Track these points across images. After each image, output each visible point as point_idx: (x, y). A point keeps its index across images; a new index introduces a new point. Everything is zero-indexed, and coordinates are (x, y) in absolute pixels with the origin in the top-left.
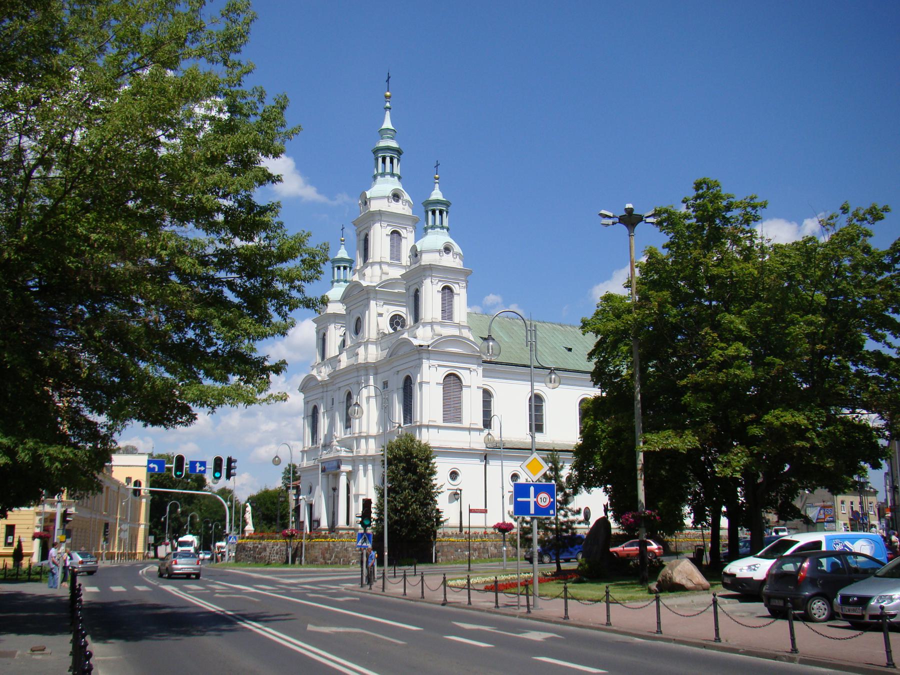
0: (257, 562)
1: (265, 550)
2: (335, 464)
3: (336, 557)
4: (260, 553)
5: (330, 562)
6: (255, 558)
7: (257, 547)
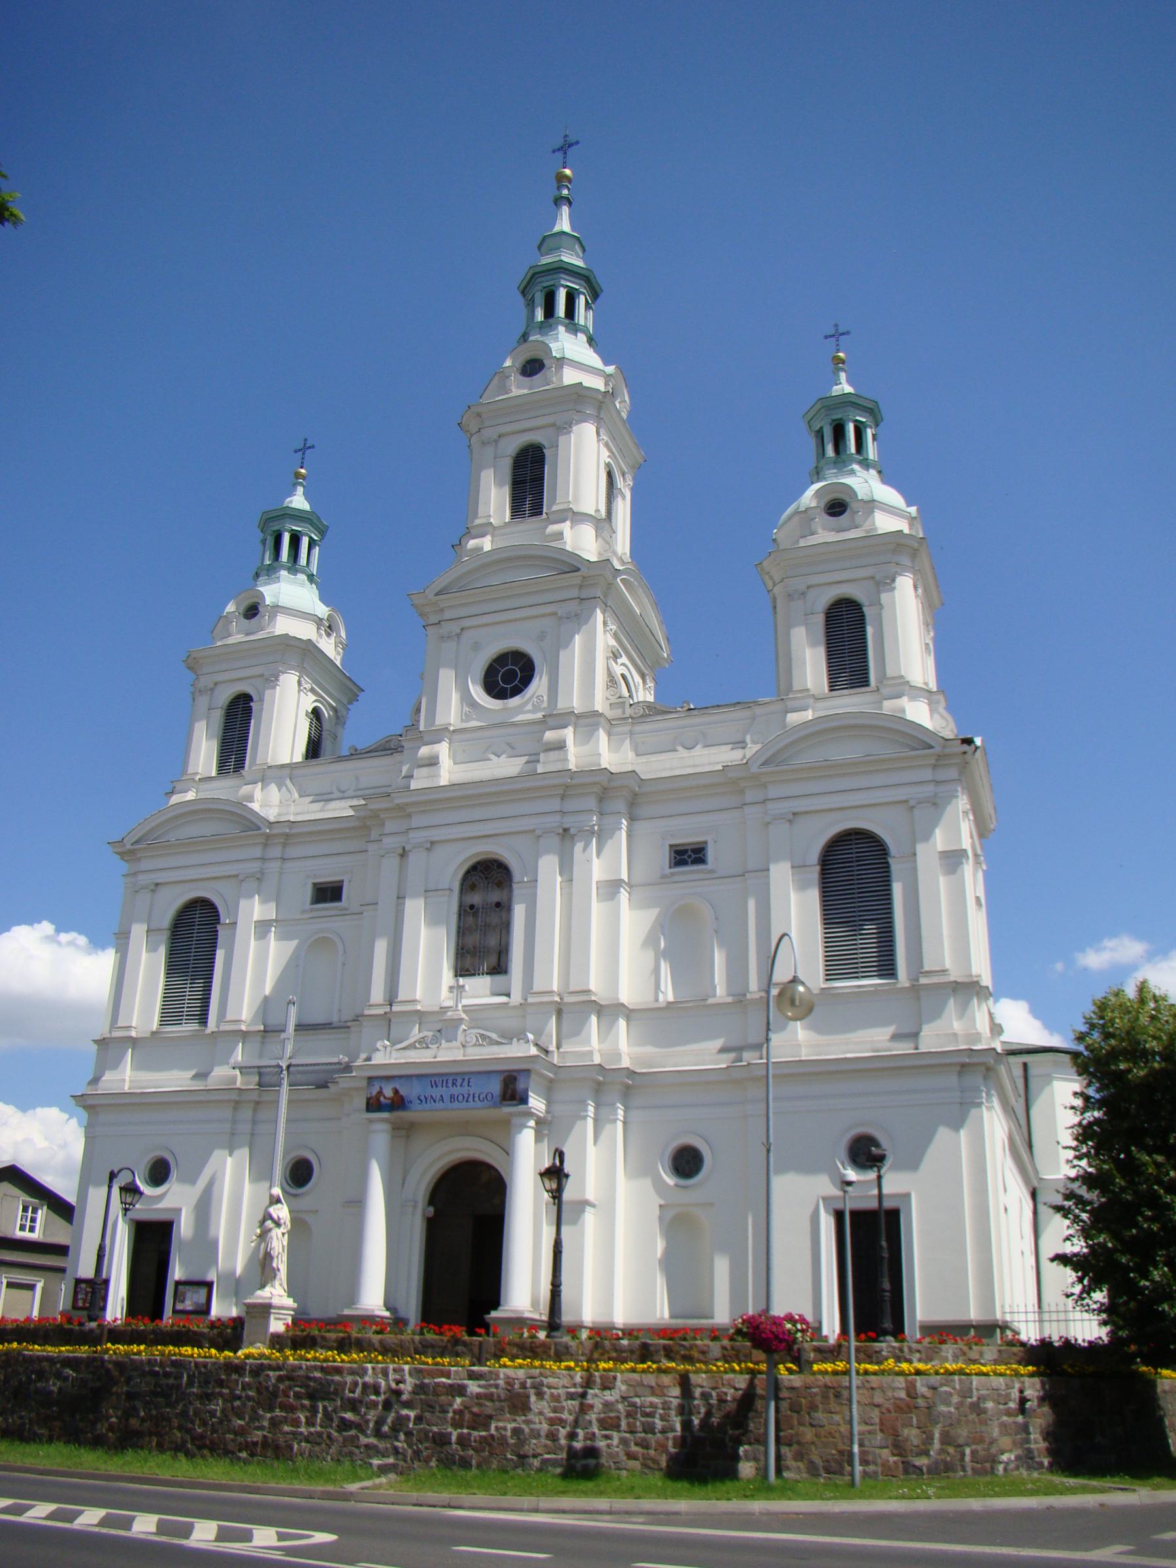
0: (448, 1462)
1: (517, 1403)
2: (496, 1087)
3: (947, 1439)
4: (481, 1421)
5: (922, 1461)
6: (441, 1440)
7: (460, 1390)
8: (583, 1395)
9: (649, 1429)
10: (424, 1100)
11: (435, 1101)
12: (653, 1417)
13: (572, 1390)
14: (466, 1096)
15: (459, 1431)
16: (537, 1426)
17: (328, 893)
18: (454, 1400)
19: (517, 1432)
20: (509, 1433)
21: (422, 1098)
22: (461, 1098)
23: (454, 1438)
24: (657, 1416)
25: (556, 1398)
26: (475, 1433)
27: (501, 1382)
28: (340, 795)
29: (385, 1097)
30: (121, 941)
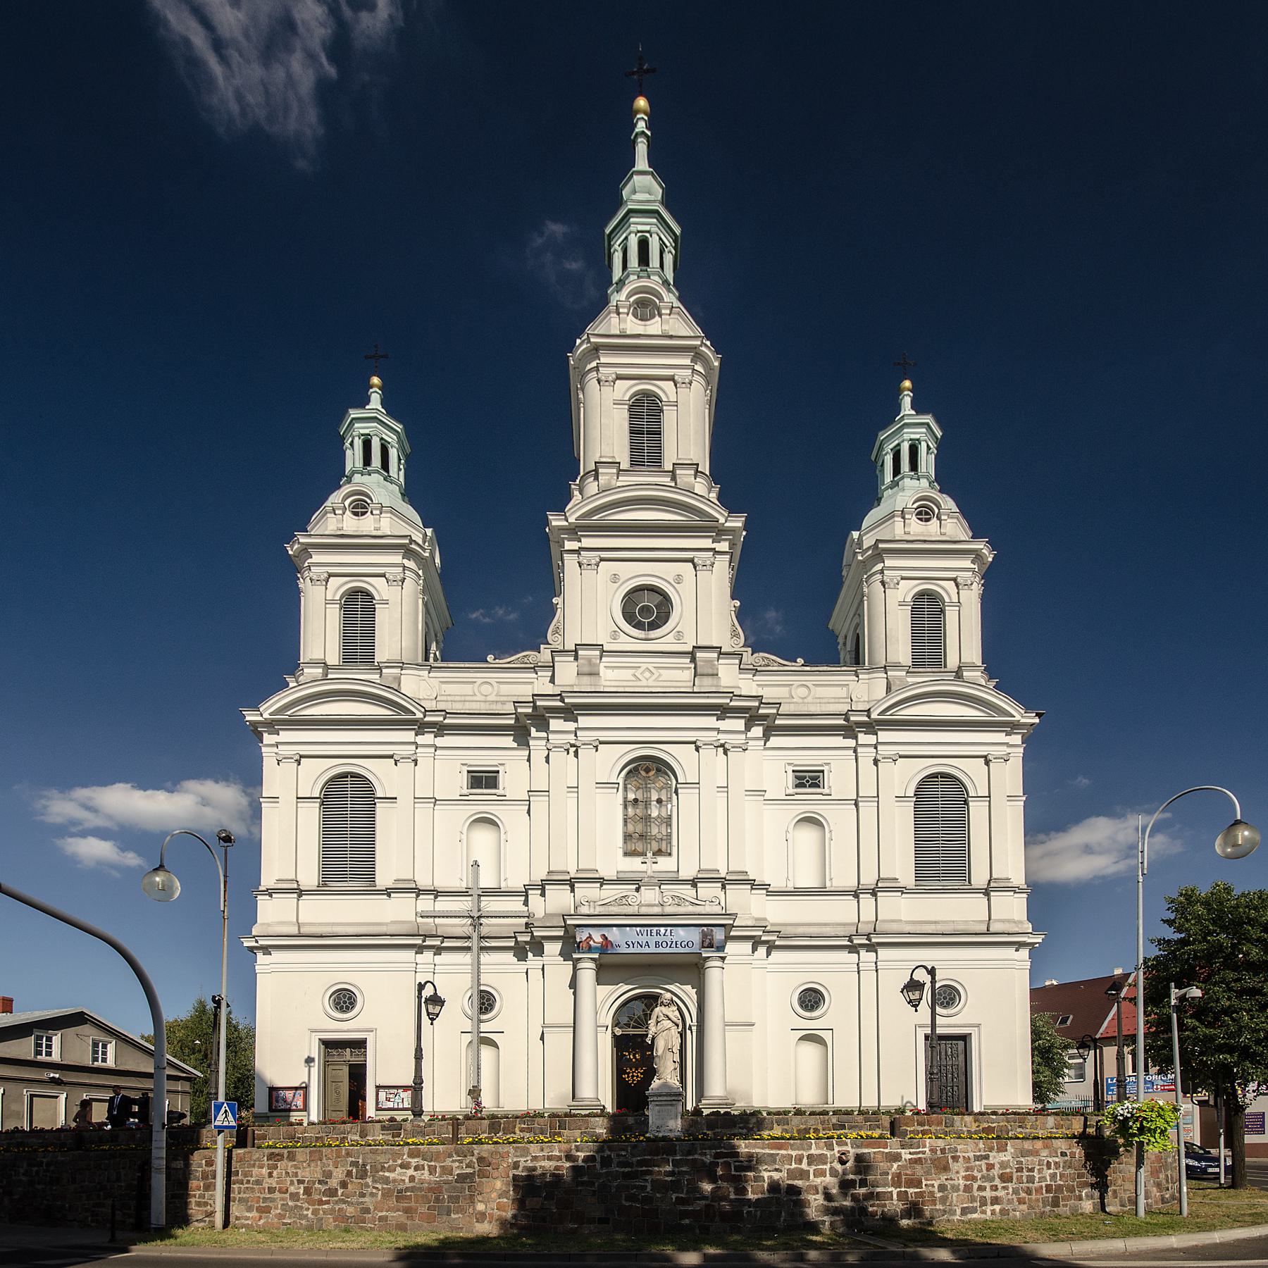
8: (987, 1157)
9: (1031, 1180)
10: (631, 945)
11: (641, 946)
12: (1033, 1172)
13: (978, 1154)
14: (669, 943)
15: (898, 1189)
16: (956, 1182)
17: (483, 780)
18: (892, 1166)
19: (942, 1188)
20: (936, 1189)
21: (630, 943)
22: (664, 945)
23: (895, 1196)
24: (1036, 1170)
25: (967, 1160)
26: (911, 1190)
27: (927, 1150)
28: (483, 698)
29: (594, 942)
30: (256, 732)
